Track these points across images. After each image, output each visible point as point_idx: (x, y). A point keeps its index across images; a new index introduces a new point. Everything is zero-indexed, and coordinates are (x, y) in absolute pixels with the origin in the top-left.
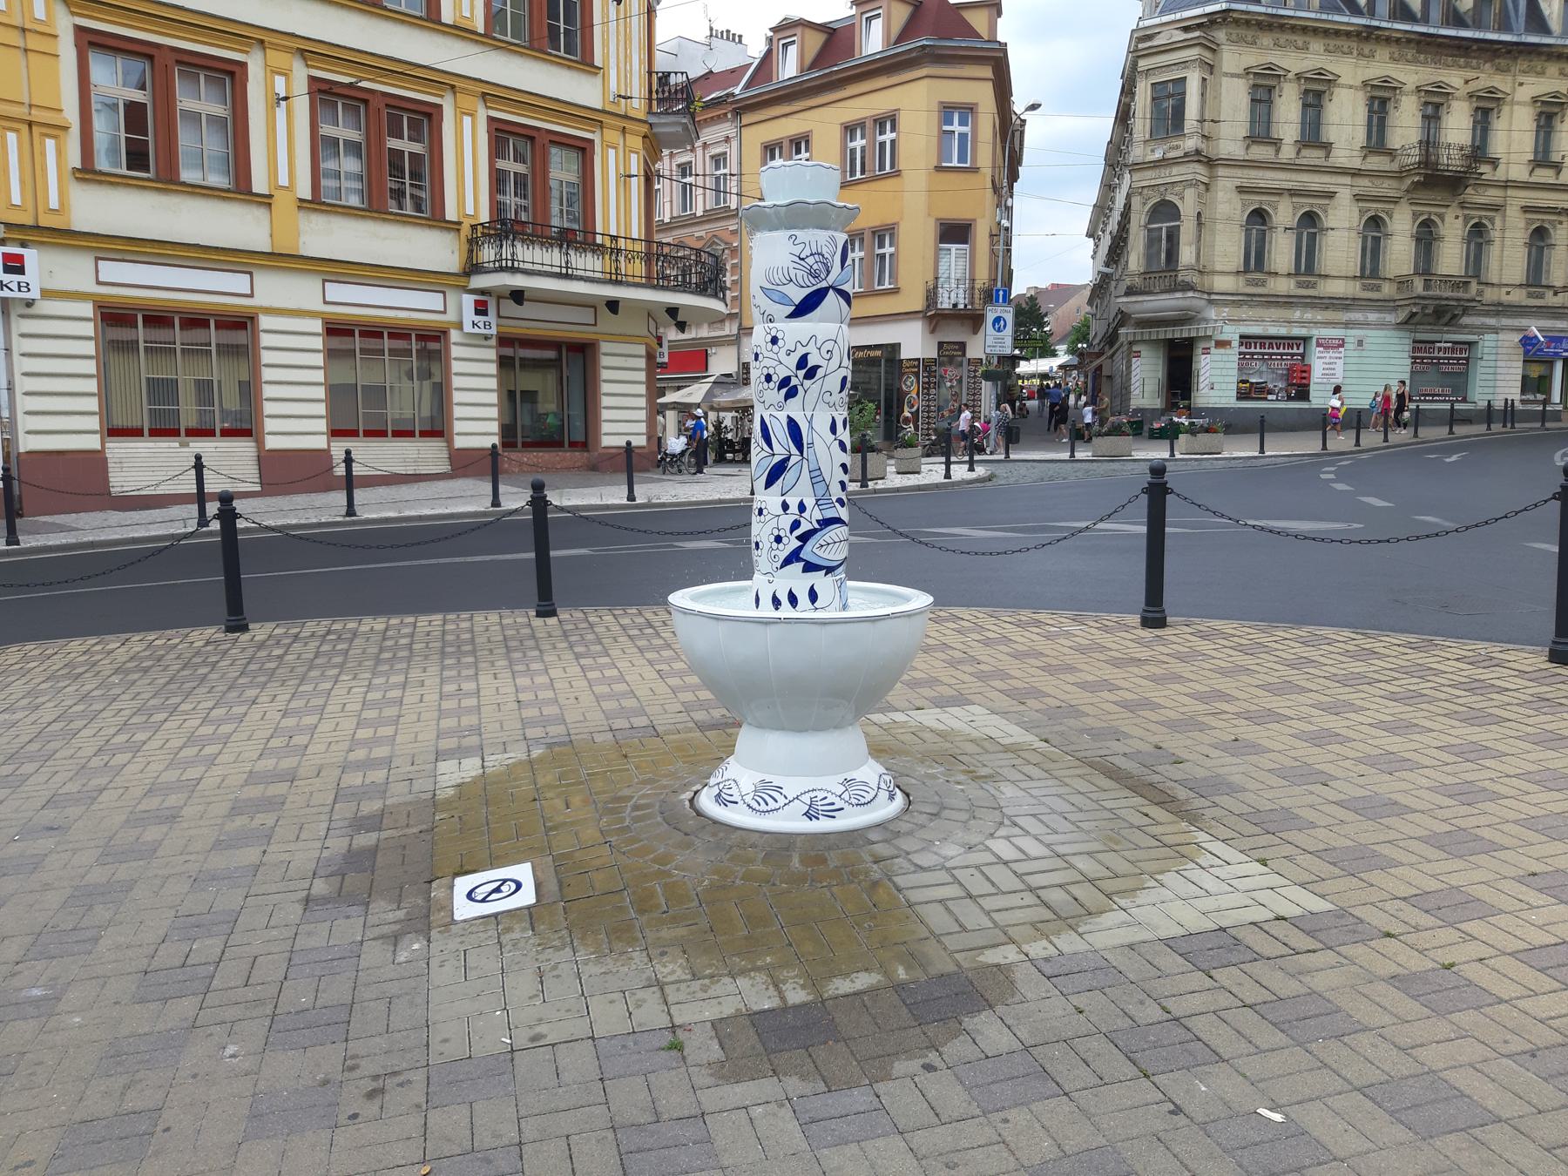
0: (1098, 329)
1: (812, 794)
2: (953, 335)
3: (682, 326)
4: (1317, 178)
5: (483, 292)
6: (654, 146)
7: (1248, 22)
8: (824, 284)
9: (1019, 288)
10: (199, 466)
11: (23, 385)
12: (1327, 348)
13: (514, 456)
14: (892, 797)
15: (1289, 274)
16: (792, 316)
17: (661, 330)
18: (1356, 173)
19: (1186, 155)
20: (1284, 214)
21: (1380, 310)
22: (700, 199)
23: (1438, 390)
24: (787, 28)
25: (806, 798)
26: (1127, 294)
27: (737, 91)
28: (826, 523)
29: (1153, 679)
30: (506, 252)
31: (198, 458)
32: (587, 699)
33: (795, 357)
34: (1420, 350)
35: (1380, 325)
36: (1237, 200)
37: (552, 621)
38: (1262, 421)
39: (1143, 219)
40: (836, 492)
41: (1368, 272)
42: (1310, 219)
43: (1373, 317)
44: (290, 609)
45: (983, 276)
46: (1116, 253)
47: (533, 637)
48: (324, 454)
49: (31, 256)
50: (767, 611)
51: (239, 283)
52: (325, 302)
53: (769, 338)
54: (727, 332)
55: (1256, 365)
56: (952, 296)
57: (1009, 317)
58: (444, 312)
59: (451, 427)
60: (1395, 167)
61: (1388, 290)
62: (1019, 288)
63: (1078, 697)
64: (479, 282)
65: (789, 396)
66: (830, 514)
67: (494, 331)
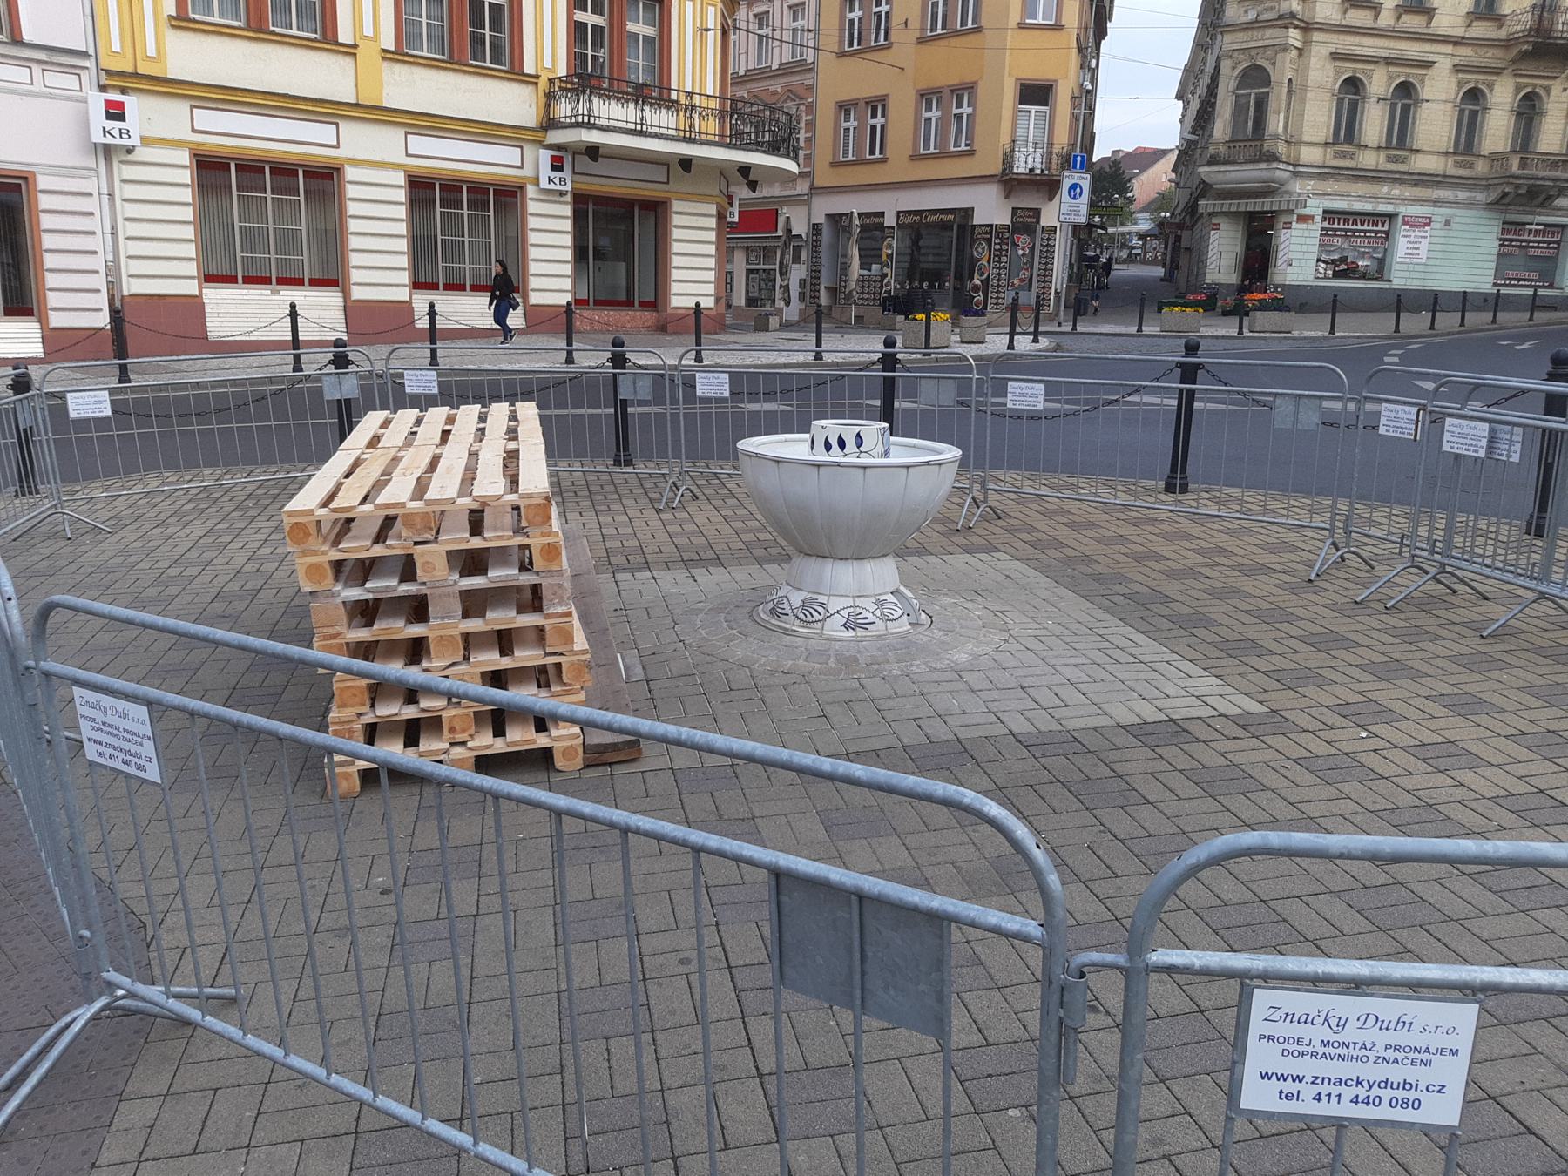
0: (1183, 198)
2: (1027, 201)
3: (753, 186)
4: (1416, 46)
5: (558, 147)
9: (1100, 152)
10: (293, 314)
12: (1412, 226)
13: (586, 313)
17: (732, 189)
18: (1458, 42)
19: (1280, 17)
20: (1379, 83)
21: (1471, 188)
22: (776, 51)
23: (1525, 275)
26: (1210, 163)
29: (1165, 536)
30: (583, 107)
31: (293, 306)
32: (662, 536)
34: (1509, 232)
35: (1471, 204)
36: (1330, 67)
38: (1335, 301)
39: (1232, 84)
41: (1462, 147)
42: (1406, 90)
43: (1462, 195)
45: (1062, 140)
46: (1201, 120)
48: (407, 307)
49: (131, 103)
50: (822, 457)
51: (325, 133)
55: (1338, 241)
56: (1027, 161)
57: (1086, 185)
58: (521, 167)
59: (525, 282)
60: (1502, 34)
61: (1481, 168)
62: (1100, 152)
63: (1092, 548)
64: (556, 137)
67: (569, 187)
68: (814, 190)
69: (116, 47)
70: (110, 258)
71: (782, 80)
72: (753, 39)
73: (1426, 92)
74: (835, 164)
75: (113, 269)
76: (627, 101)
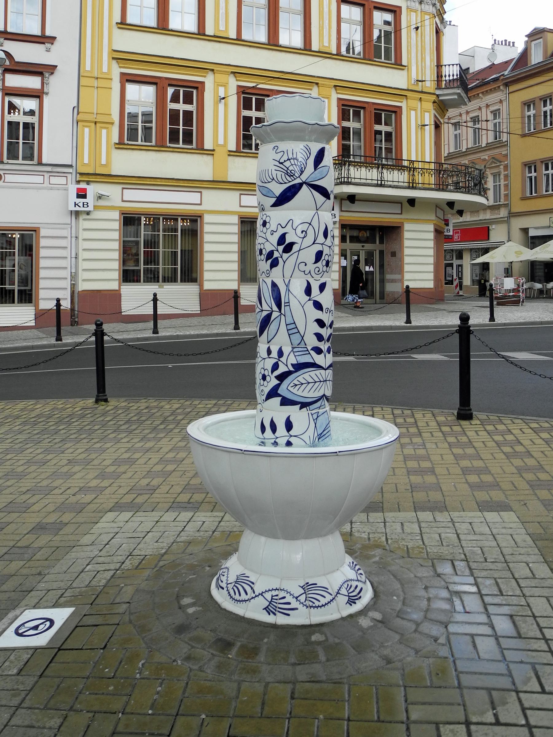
1: (274, 593)
6: (442, 106)
8: (298, 181)
10: (155, 300)
11: (83, 255)
16: (275, 205)
24: (537, 34)
25: (268, 596)
27: (506, 73)
28: (299, 367)
31: (155, 295)
33: (277, 236)
40: (312, 341)
44: (133, 392)
51: (194, 197)
52: (241, 206)
54: (501, 216)
66: (306, 359)
67: (337, 219)
68: (512, 215)
69: (86, 161)
70: (73, 271)
71: (488, 153)
72: (471, 131)
74: (524, 199)
75: (74, 277)
76: (372, 168)
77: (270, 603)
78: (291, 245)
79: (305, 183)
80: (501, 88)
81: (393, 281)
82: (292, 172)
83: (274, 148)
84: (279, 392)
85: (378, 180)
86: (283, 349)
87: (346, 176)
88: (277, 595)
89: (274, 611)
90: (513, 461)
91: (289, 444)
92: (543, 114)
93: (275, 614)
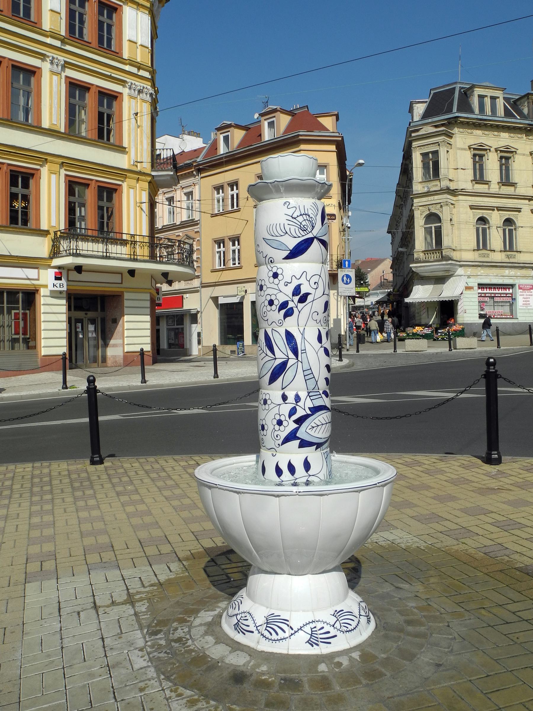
1: (312, 625)
3: (170, 283)
5: (59, 267)
6: (154, 187)
7: (468, 123)
8: (310, 236)
14: (369, 621)
15: (501, 251)
20: (496, 219)
25: (308, 629)
28: (315, 410)
37: (100, 467)
42: (509, 222)
47: (89, 479)
53: (271, 274)
58: (122, 283)
64: (57, 262)
65: (286, 315)
67: (65, 289)
73: (519, 223)
74: (214, 271)
77: (311, 635)
78: (307, 295)
79: (315, 237)
80: (194, 173)
81: (115, 346)
82: (305, 226)
83: (285, 203)
84: (297, 435)
85: (103, 252)
86: (300, 394)
87: (74, 248)
88: (315, 627)
89: (317, 642)
90: (190, 502)
91: (307, 483)
92: (230, 197)
93: (317, 645)
